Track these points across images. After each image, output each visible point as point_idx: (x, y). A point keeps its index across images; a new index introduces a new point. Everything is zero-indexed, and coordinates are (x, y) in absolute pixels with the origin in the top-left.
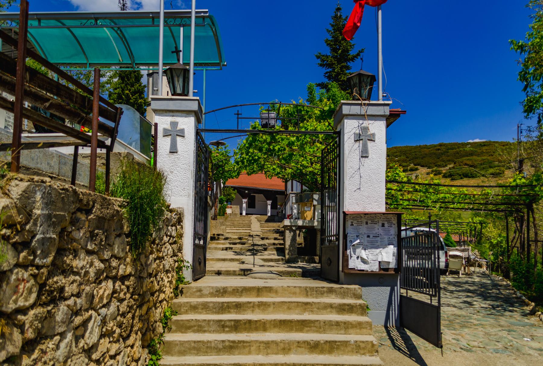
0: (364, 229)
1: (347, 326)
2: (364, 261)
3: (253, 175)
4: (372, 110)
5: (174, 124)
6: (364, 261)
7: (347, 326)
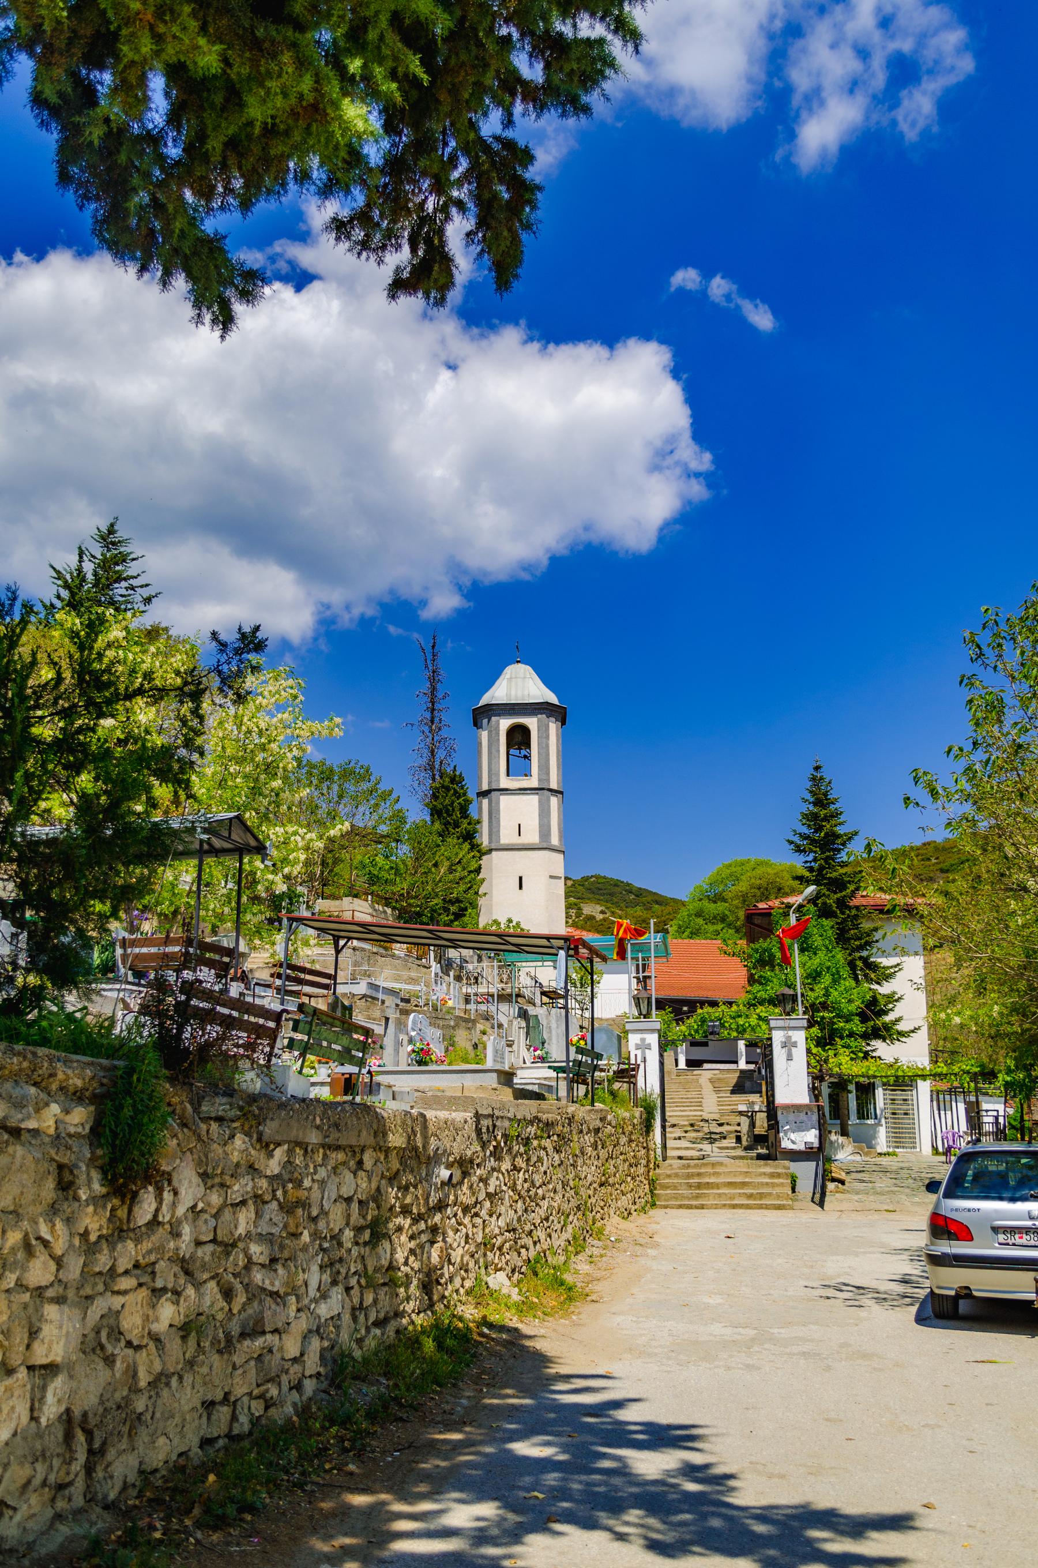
0: (792, 1117)
1: (773, 1185)
2: (793, 1142)
3: (710, 1085)
4: (793, 1023)
5: (643, 1040)
6: (793, 1142)
7: (773, 1185)
